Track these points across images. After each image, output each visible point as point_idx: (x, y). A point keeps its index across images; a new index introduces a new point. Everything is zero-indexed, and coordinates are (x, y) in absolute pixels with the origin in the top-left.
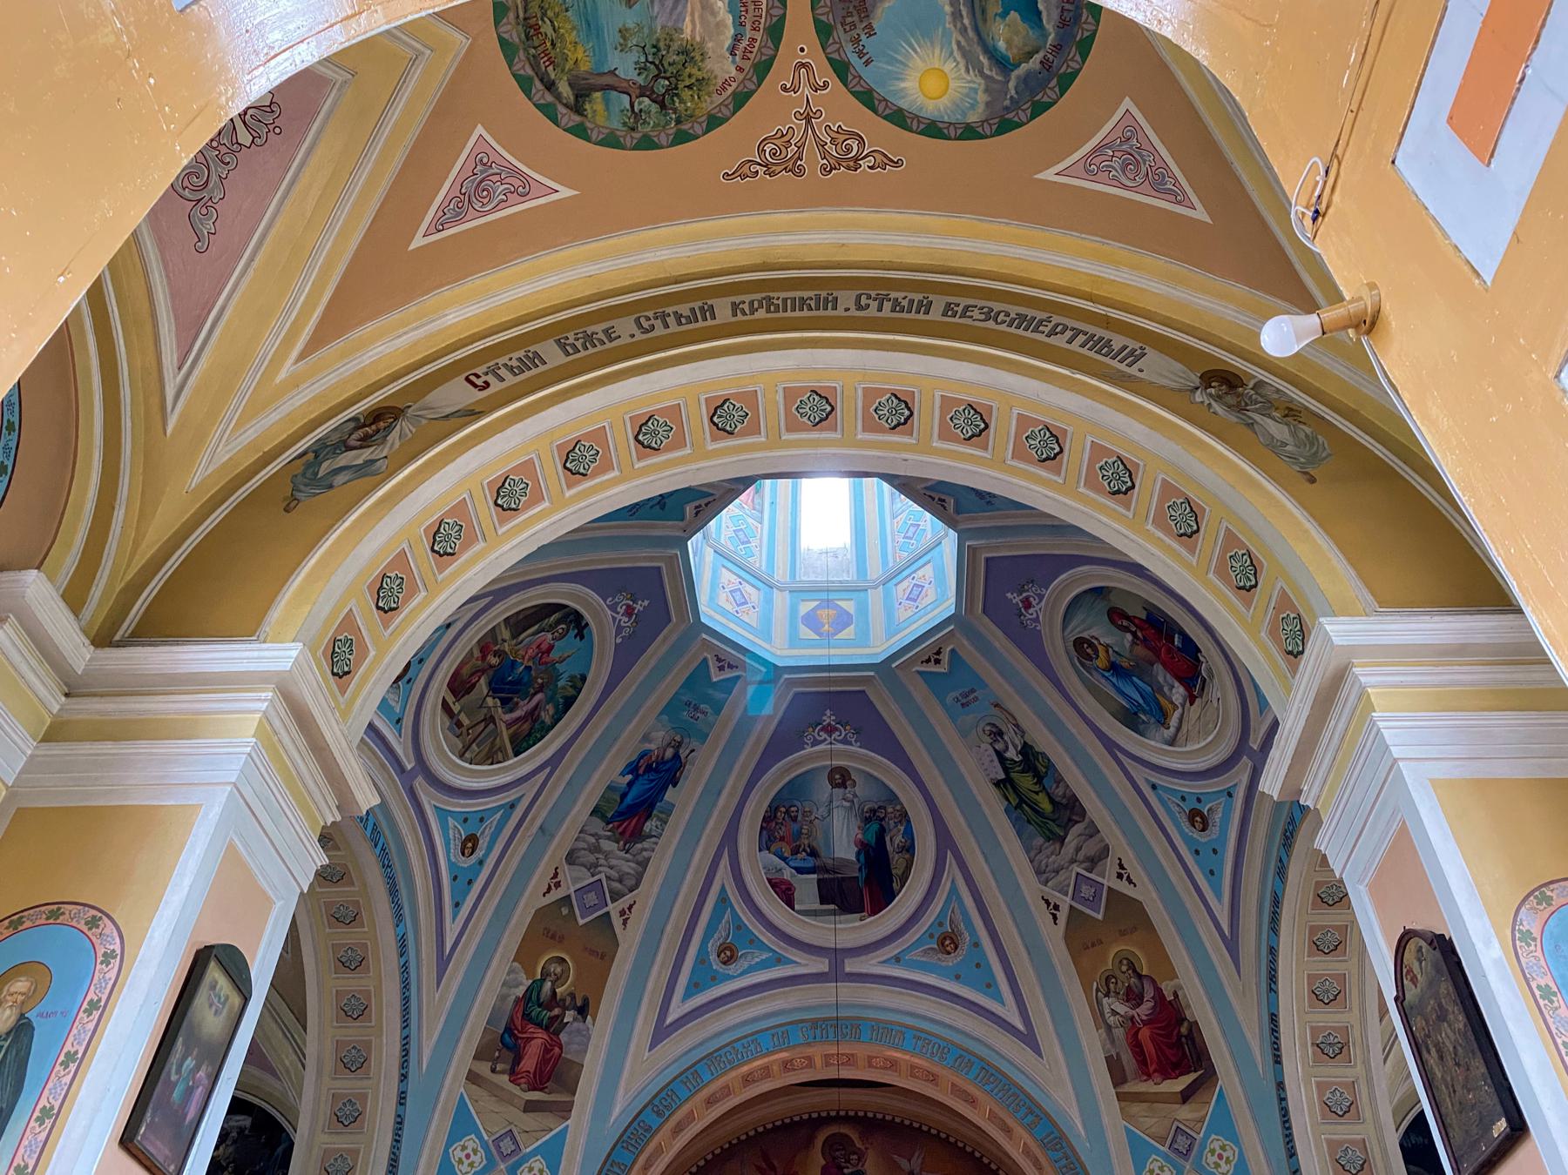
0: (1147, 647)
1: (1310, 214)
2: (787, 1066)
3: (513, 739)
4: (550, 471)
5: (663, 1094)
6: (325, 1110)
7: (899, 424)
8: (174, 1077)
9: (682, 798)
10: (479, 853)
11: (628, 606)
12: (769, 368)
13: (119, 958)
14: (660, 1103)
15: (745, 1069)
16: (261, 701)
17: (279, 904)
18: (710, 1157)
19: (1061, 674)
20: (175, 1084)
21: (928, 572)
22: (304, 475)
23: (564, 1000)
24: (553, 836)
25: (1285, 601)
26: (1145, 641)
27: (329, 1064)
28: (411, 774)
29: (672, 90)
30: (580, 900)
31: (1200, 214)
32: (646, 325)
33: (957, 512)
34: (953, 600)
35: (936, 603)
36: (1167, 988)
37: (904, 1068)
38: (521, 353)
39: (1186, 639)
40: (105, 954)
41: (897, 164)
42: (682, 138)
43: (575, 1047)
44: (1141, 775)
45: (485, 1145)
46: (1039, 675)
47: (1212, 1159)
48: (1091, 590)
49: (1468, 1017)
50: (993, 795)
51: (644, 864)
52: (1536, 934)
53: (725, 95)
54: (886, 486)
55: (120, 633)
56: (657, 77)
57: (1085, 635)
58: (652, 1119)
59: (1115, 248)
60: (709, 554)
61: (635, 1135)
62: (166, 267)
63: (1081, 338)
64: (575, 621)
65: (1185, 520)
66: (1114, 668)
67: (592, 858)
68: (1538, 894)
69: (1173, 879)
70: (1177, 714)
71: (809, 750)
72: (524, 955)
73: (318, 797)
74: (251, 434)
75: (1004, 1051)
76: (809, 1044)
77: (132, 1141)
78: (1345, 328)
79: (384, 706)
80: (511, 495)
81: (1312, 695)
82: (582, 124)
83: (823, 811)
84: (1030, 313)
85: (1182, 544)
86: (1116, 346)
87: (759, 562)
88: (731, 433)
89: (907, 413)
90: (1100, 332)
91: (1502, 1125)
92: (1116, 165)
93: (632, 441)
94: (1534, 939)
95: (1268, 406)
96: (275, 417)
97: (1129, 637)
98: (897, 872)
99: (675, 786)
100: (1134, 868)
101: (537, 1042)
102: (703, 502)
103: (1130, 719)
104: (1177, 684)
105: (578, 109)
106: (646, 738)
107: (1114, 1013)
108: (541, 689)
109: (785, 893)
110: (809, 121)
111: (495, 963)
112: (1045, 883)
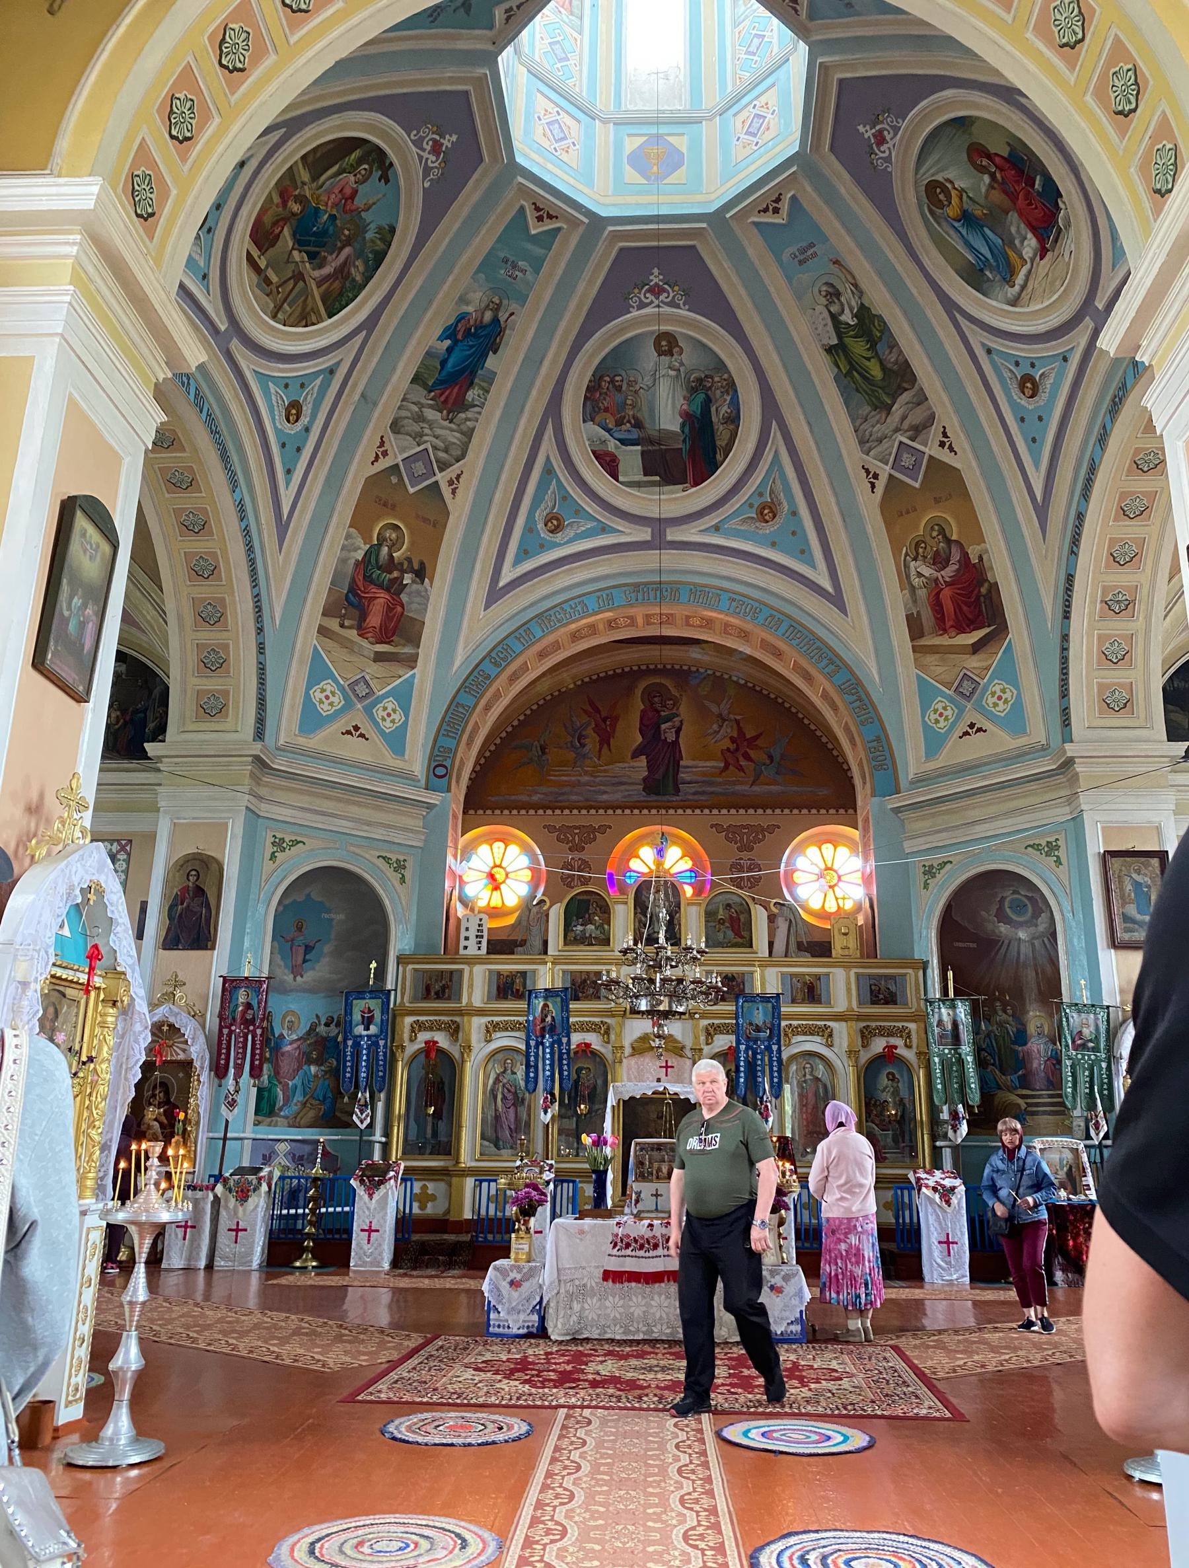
0: (1005, 192)
2: (611, 624)
3: (324, 299)
8: (66, 613)
9: (504, 365)
10: (304, 420)
11: (435, 141)
15: (573, 626)
16: (69, 246)
19: (911, 234)
21: (771, 98)
23: (402, 564)
24: (375, 404)
25: (1164, 128)
27: (189, 619)
28: (227, 335)
33: (811, 17)
36: (973, 552)
39: (1049, 181)
50: (824, 360)
51: (469, 434)
57: (939, 177)
58: (488, 667)
64: (377, 159)
66: (966, 217)
69: (995, 448)
70: (1024, 270)
71: (635, 313)
72: (360, 521)
73: (145, 351)
76: (631, 606)
83: (648, 381)
97: (987, 179)
99: (495, 352)
103: (975, 277)
104: (1030, 235)
106: (463, 300)
107: (920, 575)
108: (348, 242)
109: (610, 464)
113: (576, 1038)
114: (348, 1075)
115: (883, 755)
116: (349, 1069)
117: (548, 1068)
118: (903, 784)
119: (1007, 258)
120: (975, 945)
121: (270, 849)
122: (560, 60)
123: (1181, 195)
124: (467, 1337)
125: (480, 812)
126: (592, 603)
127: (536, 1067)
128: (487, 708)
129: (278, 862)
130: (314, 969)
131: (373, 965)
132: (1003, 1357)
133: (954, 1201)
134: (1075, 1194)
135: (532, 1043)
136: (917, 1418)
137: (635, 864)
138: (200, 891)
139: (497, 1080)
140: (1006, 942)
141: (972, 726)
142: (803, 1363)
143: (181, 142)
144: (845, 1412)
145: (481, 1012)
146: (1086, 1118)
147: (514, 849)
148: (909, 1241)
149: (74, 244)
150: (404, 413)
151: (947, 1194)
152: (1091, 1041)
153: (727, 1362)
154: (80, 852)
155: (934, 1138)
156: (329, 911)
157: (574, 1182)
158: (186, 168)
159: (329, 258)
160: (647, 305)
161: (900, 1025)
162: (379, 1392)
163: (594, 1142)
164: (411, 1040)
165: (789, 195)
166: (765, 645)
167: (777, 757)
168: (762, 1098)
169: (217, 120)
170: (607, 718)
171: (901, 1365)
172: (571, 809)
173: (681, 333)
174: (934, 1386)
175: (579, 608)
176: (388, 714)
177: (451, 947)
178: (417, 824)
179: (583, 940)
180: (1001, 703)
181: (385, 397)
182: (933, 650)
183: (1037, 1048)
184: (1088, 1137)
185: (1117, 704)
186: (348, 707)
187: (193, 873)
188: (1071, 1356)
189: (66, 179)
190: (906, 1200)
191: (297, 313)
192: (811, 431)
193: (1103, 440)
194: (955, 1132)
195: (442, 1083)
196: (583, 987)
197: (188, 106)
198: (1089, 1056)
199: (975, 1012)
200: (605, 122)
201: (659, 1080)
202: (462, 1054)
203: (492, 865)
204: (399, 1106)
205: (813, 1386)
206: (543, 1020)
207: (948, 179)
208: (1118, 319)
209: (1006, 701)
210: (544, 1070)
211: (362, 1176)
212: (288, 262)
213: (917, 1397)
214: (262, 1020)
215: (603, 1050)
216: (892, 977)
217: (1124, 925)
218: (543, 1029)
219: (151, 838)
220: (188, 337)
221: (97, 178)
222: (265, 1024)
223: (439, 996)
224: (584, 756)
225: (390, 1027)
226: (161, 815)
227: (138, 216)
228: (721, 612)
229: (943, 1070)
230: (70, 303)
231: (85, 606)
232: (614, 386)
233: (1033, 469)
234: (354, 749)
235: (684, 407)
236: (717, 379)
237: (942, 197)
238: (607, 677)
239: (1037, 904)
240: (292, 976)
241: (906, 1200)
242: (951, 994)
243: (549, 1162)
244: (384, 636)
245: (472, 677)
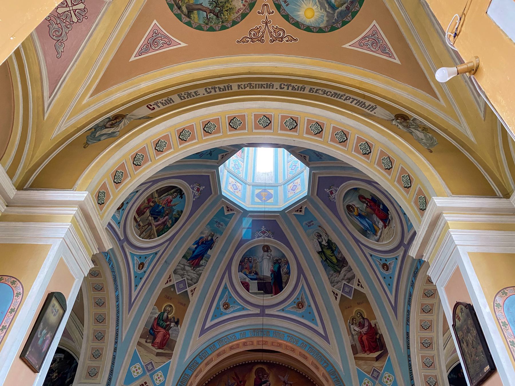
0: (371, 208)
1: (453, 35)
2: (245, 344)
4: (174, 139)
5: (203, 352)
6: (89, 353)
7: (293, 128)
8: (39, 336)
9: (213, 253)
10: (144, 269)
11: (198, 188)
12: (250, 107)
13: (22, 295)
14: (202, 355)
15: (231, 344)
16: (73, 211)
17: (77, 280)
18: (217, 374)
20: (39, 339)
21: (299, 181)
22: (91, 136)
23: (171, 319)
24: (169, 264)
25: (420, 192)
26: (370, 207)
27: (91, 337)
28: (122, 241)
29: (221, 12)
31: (397, 61)
32: (208, 91)
33: (310, 161)
34: (307, 191)
35: (301, 192)
36: (373, 323)
37: (284, 346)
38: (166, 99)
39: (384, 206)
40: (17, 293)
41: (296, 40)
42: (224, 28)
43: (174, 335)
44: (367, 251)
46: (334, 216)
47: (385, 380)
48: (354, 189)
49: (477, 330)
51: (200, 275)
52: (502, 305)
53: (239, 14)
54: (286, 151)
55: (26, 186)
56: (216, 7)
57: (350, 204)
58: (189, 372)
59: (367, 71)
61: (193, 365)
62: (46, 62)
63: (355, 102)
64: (180, 192)
65: (388, 164)
66: (359, 215)
67: (182, 272)
68: (503, 292)
69: (376, 286)
70: (380, 232)
71: (256, 239)
72: (158, 304)
74: (73, 121)
77: (24, 356)
78: (466, 72)
79: (114, 217)
80: (160, 146)
82: (190, 21)
84: (339, 92)
85: (386, 172)
86: (367, 105)
87: (242, 175)
90: (361, 100)
91: (488, 368)
92: (370, 44)
93: (202, 130)
94: (501, 306)
95: (417, 127)
96: (82, 116)
97: (365, 205)
98: (284, 281)
100: (363, 282)
101: (162, 332)
102: (224, 154)
103: (364, 232)
104: (380, 221)
105: (189, 16)
106: (202, 233)
107: (355, 330)
108: (167, 215)
109: (246, 286)
110: (266, 24)
111: (148, 306)
112: (333, 286)
119: (374, 227)
128: (196, 376)
150: (179, 268)
169: (130, 178)
173: (272, 246)
175: (233, 337)
186: (144, 373)
227: (98, 203)
244: (162, 346)
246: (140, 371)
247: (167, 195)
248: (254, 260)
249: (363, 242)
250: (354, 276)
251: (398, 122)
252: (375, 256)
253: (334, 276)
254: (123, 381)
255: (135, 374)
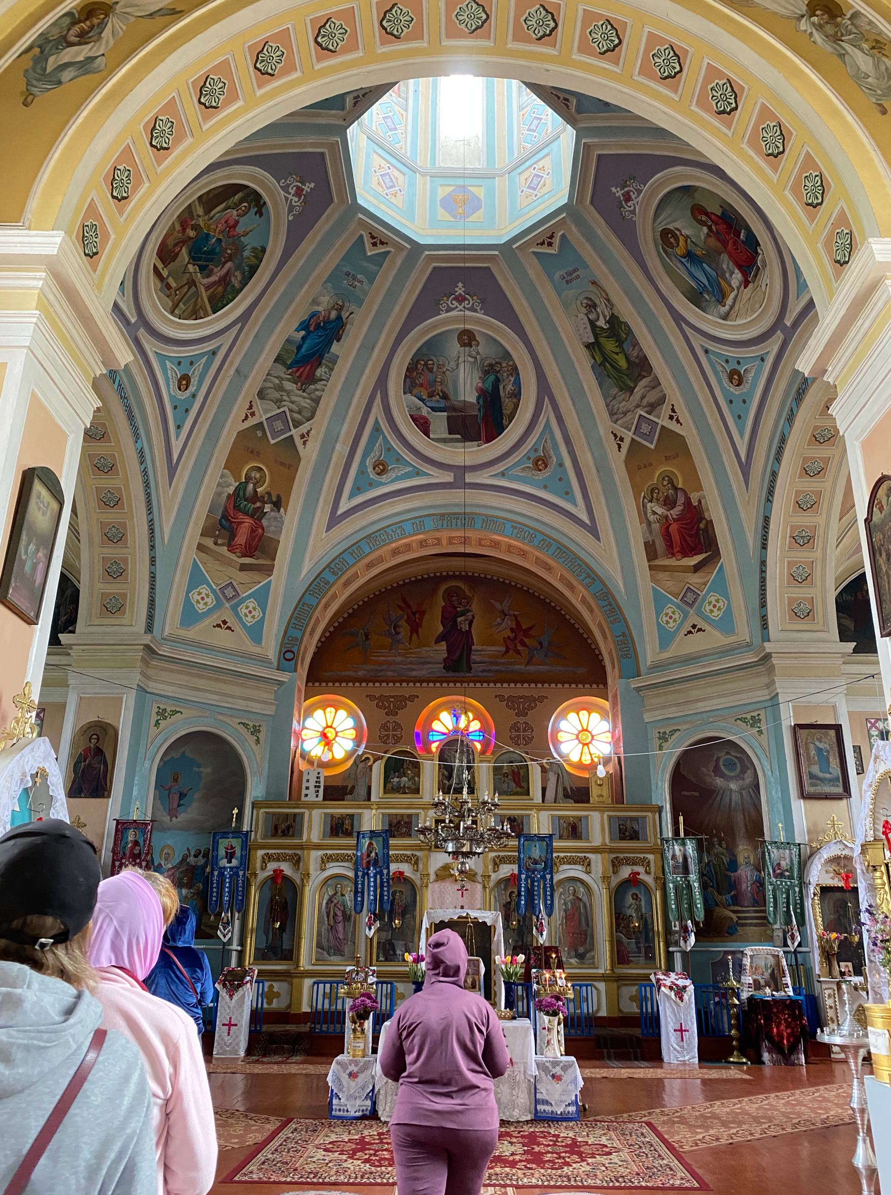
0: (718, 240)
2: (422, 544)
3: (210, 300)
4: (243, 72)
5: (337, 561)
7: (544, 35)
8: (24, 557)
9: (344, 350)
10: (192, 389)
11: (298, 188)
14: (336, 566)
15: (394, 545)
16: (36, 281)
19: (647, 258)
21: (546, 163)
23: (263, 497)
24: (246, 377)
25: (842, 218)
26: (717, 235)
27: (97, 538)
28: (135, 325)
30: (271, 426)
33: (578, 111)
36: (694, 497)
37: (505, 546)
39: (751, 235)
44: (698, 342)
45: (213, 591)
47: (708, 608)
50: (584, 353)
51: (317, 401)
57: (670, 227)
58: (328, 576)
60: (363, 141)
64: (255, 200)
66: (689, 255)
67: (277, 395)
69: (710, 421)
70: (733, 295)
71: (444, 315)
72: (232, 464)
73: (88, 355)
75: (573, 536)
76: (438, 530)
80: (211, 93)
81: (852, 296)
83: (453, 364)
88: (397, 37)
89: (552, 24)
93: (312, 43)
97: (705, 229)
98: (506, 412)
99: (338, 341)
100: (683, 413)
103: (696, 298)
104: (737, 271)
106: (315, 302)
107: (654, 513)
108: (230, 258)
109: (424, 426)
111: (209, 471)
113: (394, 867)
114: (214, 899)
115: (627, 647)
116: (215, 894)
117: (372, 893)
118: (643, 669)
119: (719, 285)
120: (697, 794)
121: (155, 717)
122: (391, 130)
123: (857, 270)
124: (314, 1119)
125: (317, 684)
126: (408, 527)
127: (363, 893)
128: (326, 607)
129: (161, 727)
130: (185, 811)
131: (235, 811)
132: (732, 1131)
133: (686, 997)
134: (777, 991)
135: (360, 874)
136: (673, 1188)
137: (436, 725)
138: (99, 751)
139: (330, 901)
140: (721, 792)
141: (694, 626)
142: (580, 1139)
143: (119, 201)
144: (617, 1184)
145: (318, 847)
146: (784, 931)
147: (342, 713)
148: (651, 1026)
149: (41, 279)
150: (269, 385)
151: (680, 991)
152: (787, 870)
153: (521, 1140)
154: (29, 747)
155: (667, 945)
156: (199, 766)
157: (391, 983)
158: (122, 219)
159: (216, 270)
160: (453, 309)
161: (642, 856)
162: (251, 1172)
163: (414, 959)
164: (263, 869)
165: (560, 234)
166: (538, 562)
167: (545, 645)
168: (538, 917)
169: (147, 185)
170: (416, 612)
171: (651, 1137)
172: (388, 682)
173: (479, 331)
174: (682, 1157)
175: (398, 531)
176: (249, 611)
177: (295, 793)
178: (269, 697)
179: (399, 790)
180: (715, 610)
181: (254, 371)
182: (664, 568)
183: (746, 874)
184: (785, 945)
185: (802, 613)
186: (218, 606)
187: (95, 737)
188: (783, 1129)
189: (36, 232)
190: (649, 995)
191: (190, 309)
192: (574, 405)
193: (791, 418)
194: (686, 942)
195: (286, 903)
196: (399, 826)
197: (126, 175)
198: (786, 882)
199: (700, 848)
200: (424, 175)
201: (462, 907)
202: (302, 880)
203: (325, 725)
204: (252, 920)
205: (590, 1160)
206: (369, 856)
207: (676, 232)
208: (810, 350)
209: (719, 609)
210: (369, 895)
211: (224, 980)
212: (184, 273)
213: (671, 1169)
214: (147, 854)
215: (413, 877)
216: (636, 819)
217: (810, 781)
218: (368, 863)
219: (62, 707)
220: (120, 344)
221: (60, 232)
222: (149, 858)
223: (285, 833)
224: (398, 641)
225: (246, 862)
226: (70, 690)
227: (86, 255)
228: (507, 536)
229: (676, 894)
230: (36, 324)
231: (37, 550)
232: (428, 368)
233: (739, 438)
234: (222, 638)
235: (480, 385)
236: (504, 365)
237: (672, 240)
238: (417, 581)
239: (741, 761)
240: (169, 817)
241: (649, 995)
242: (682, 834)
243: (372, 968)
244: (249, 550)
245: (315, 583)
246: (211, 601)
247: (792, 860)
248: (439, 366)
249: (692, 320)
250: (662, 400)
251: (813, 24)
252: (714, 353)
253: (618, 399)
254: (178, 620)
255: (201, 606)
